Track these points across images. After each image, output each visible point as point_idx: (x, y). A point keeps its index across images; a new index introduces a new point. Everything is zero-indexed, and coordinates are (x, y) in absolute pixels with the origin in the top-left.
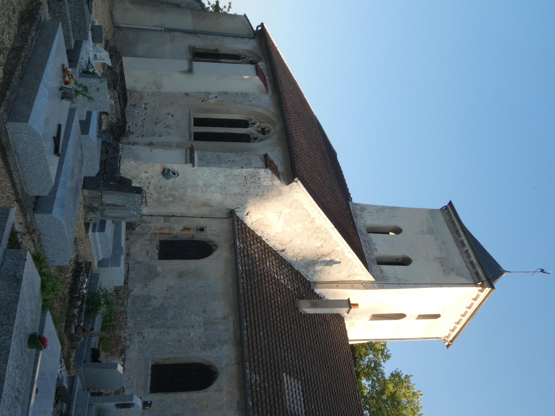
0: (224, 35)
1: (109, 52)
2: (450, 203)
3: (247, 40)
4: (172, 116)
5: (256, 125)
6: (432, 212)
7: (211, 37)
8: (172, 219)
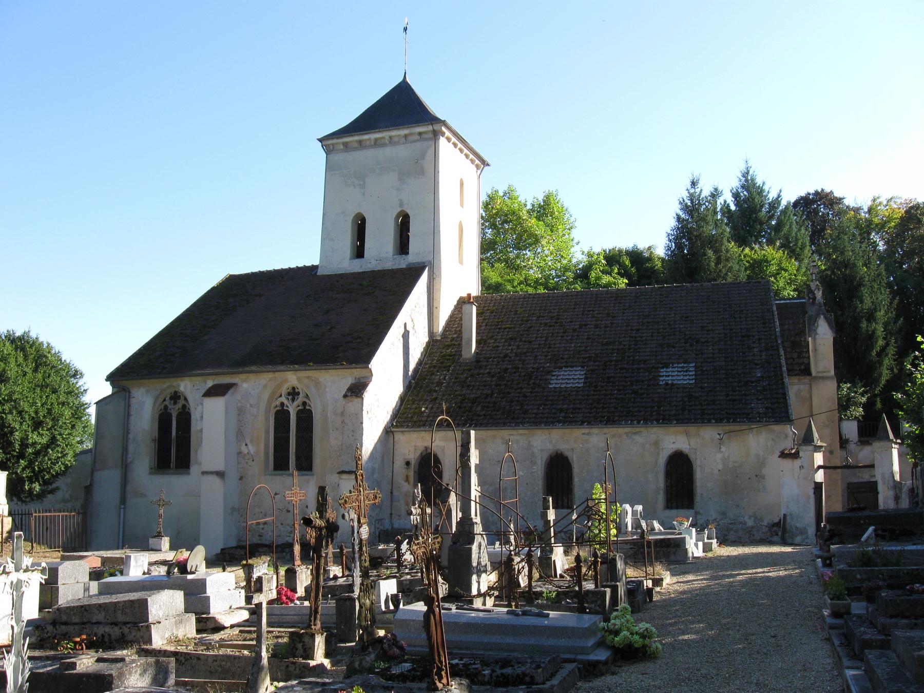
0: (126, 430)
1: (658, 559)
2: (320, 140)
3: (133, 401)
4: (276, 494)
5: (286, 402)
6: (329, 168)
7: (131, 448)
8: (396, 493)
